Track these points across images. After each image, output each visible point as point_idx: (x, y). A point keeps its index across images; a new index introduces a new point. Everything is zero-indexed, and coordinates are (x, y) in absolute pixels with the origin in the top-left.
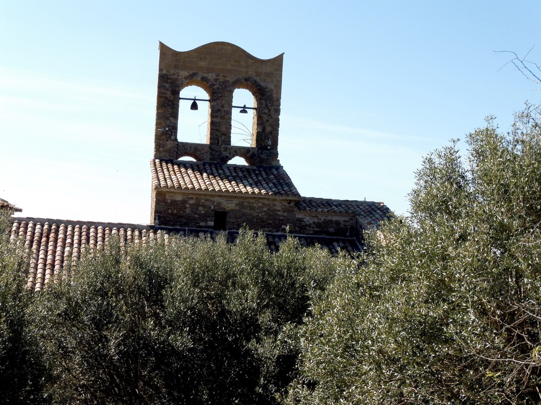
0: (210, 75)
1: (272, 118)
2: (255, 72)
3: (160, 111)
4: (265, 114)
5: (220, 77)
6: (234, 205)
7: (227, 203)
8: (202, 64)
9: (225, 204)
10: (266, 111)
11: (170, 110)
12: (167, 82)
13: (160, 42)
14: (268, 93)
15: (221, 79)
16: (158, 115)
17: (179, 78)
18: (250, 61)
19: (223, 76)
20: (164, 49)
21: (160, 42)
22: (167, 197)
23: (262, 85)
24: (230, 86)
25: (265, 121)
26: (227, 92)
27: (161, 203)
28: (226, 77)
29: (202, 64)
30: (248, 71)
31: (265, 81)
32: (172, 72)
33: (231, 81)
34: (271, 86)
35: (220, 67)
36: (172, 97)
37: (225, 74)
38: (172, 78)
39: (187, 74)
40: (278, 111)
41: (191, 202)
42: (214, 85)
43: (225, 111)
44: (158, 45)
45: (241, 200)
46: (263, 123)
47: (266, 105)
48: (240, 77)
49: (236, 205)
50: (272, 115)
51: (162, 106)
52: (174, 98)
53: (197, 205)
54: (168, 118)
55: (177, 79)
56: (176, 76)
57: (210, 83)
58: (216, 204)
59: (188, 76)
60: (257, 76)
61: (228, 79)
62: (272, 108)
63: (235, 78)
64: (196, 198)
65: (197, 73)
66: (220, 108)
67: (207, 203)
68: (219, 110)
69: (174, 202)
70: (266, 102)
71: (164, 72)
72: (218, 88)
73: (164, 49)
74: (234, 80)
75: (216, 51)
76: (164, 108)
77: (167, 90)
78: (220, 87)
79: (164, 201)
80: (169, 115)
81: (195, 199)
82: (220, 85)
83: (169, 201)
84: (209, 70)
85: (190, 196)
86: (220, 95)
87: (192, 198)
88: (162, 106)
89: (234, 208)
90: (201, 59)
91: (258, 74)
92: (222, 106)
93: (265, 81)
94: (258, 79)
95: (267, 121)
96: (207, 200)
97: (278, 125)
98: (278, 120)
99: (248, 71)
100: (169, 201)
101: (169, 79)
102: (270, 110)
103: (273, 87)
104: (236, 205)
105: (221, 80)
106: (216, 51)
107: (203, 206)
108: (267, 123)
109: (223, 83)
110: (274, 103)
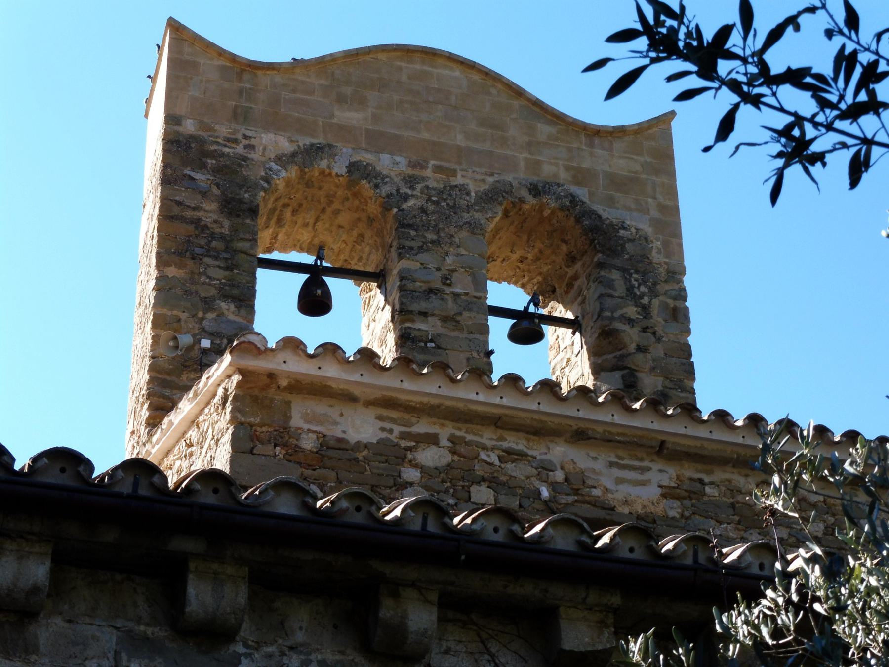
0: (385, 158)
1: (659, 340)
2: (567, 168)
3: (171, 271)
4: (630, 321)
5: (428, 173)
6: (651, 493)
7: (619, 481)
8: (351, 117)
9: (608, 483)
10: (632, 311)
11: (219, 274)
12: (202, 167)
13: (175, 26)
14: (629, 246)
15: (433, 179)
16: (163, 286)
17: (255, 156)
18: (544, 130)
19: (438, 169)
20: (188, 52)
21: (175, 26)
22: (297, 421)
23: (605, 215)
24: (469, 208)
25: (632, 347)
26: (460, 228)
27: (269, 449)
28: (454, 173)
29: (351, 117)
30: (538, 163)
31: (611, 202)
32: (223, 130)
33: (472, 187)
34: (640, 224)
35: (425, 135)
36: (226, 223)
37: (445, 164)
38: (222, 155)
39: (285, 145)
40: (679, 316)
41: (429, 456)
42: (406, 198)
43: (456, 296)
44: (159, 33)
45: (689, 471)
46: (622, 357)
47: (630, 289)
48: (509, 178)
49: (668, 493)
50: (660, 332)
51: (180, 254)
52: (234, 229)
53: (459, 478)
54: (208, 304)
55: (245, 159)
56: (240, 149)
57: (385, 190)
58: (559, 476)
59: (294, 155)
60: (578, 183)
61: (459, 180)
62: (656, 302)
63: (491, 180)
64: (452, 439)
65: (330, 146)
66: (438, 285)
67: (517, 471)
68: (431, 291)
69: (334, 452)
70: (627, 280)
71: (189, 127)
72: (423, 210)
73: (188, 52)
74: (484, 187)
75: (404, 78)
76: (190, 263)
77: (204, 194)
78: (432, 208)
79: (283, 436)
80: (213, 292)
81: (444, 442)
82: (429, 199)
83: (308, 443)
84: (379, 141)
85: (422, 427)
86: (430, 236)
87: (432, 440)
88: (180, 254)
89: (658, 510)
90: (341, 100)
91: (581, 176)
92: (446, 280)
93: (611, 202)
94: (582, 193)
95: (641, 349)
96: (510, 455)
97: (690, 371)
98: (687, 351)
99: (538, 163)
100: (308, 443)
101: (213, 155)
102: (646, 310)
103: (647, 229)
104: (668, 493)
105: (432, 184)
106: (404, 78)
107: (493, 482)
108: (640, 356)
109: (440, 192)
110: (662, 287)
